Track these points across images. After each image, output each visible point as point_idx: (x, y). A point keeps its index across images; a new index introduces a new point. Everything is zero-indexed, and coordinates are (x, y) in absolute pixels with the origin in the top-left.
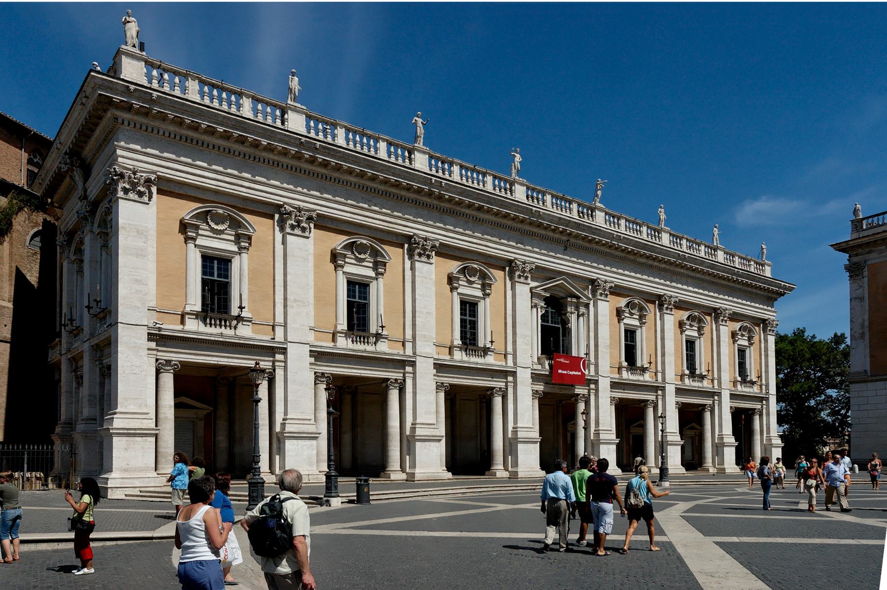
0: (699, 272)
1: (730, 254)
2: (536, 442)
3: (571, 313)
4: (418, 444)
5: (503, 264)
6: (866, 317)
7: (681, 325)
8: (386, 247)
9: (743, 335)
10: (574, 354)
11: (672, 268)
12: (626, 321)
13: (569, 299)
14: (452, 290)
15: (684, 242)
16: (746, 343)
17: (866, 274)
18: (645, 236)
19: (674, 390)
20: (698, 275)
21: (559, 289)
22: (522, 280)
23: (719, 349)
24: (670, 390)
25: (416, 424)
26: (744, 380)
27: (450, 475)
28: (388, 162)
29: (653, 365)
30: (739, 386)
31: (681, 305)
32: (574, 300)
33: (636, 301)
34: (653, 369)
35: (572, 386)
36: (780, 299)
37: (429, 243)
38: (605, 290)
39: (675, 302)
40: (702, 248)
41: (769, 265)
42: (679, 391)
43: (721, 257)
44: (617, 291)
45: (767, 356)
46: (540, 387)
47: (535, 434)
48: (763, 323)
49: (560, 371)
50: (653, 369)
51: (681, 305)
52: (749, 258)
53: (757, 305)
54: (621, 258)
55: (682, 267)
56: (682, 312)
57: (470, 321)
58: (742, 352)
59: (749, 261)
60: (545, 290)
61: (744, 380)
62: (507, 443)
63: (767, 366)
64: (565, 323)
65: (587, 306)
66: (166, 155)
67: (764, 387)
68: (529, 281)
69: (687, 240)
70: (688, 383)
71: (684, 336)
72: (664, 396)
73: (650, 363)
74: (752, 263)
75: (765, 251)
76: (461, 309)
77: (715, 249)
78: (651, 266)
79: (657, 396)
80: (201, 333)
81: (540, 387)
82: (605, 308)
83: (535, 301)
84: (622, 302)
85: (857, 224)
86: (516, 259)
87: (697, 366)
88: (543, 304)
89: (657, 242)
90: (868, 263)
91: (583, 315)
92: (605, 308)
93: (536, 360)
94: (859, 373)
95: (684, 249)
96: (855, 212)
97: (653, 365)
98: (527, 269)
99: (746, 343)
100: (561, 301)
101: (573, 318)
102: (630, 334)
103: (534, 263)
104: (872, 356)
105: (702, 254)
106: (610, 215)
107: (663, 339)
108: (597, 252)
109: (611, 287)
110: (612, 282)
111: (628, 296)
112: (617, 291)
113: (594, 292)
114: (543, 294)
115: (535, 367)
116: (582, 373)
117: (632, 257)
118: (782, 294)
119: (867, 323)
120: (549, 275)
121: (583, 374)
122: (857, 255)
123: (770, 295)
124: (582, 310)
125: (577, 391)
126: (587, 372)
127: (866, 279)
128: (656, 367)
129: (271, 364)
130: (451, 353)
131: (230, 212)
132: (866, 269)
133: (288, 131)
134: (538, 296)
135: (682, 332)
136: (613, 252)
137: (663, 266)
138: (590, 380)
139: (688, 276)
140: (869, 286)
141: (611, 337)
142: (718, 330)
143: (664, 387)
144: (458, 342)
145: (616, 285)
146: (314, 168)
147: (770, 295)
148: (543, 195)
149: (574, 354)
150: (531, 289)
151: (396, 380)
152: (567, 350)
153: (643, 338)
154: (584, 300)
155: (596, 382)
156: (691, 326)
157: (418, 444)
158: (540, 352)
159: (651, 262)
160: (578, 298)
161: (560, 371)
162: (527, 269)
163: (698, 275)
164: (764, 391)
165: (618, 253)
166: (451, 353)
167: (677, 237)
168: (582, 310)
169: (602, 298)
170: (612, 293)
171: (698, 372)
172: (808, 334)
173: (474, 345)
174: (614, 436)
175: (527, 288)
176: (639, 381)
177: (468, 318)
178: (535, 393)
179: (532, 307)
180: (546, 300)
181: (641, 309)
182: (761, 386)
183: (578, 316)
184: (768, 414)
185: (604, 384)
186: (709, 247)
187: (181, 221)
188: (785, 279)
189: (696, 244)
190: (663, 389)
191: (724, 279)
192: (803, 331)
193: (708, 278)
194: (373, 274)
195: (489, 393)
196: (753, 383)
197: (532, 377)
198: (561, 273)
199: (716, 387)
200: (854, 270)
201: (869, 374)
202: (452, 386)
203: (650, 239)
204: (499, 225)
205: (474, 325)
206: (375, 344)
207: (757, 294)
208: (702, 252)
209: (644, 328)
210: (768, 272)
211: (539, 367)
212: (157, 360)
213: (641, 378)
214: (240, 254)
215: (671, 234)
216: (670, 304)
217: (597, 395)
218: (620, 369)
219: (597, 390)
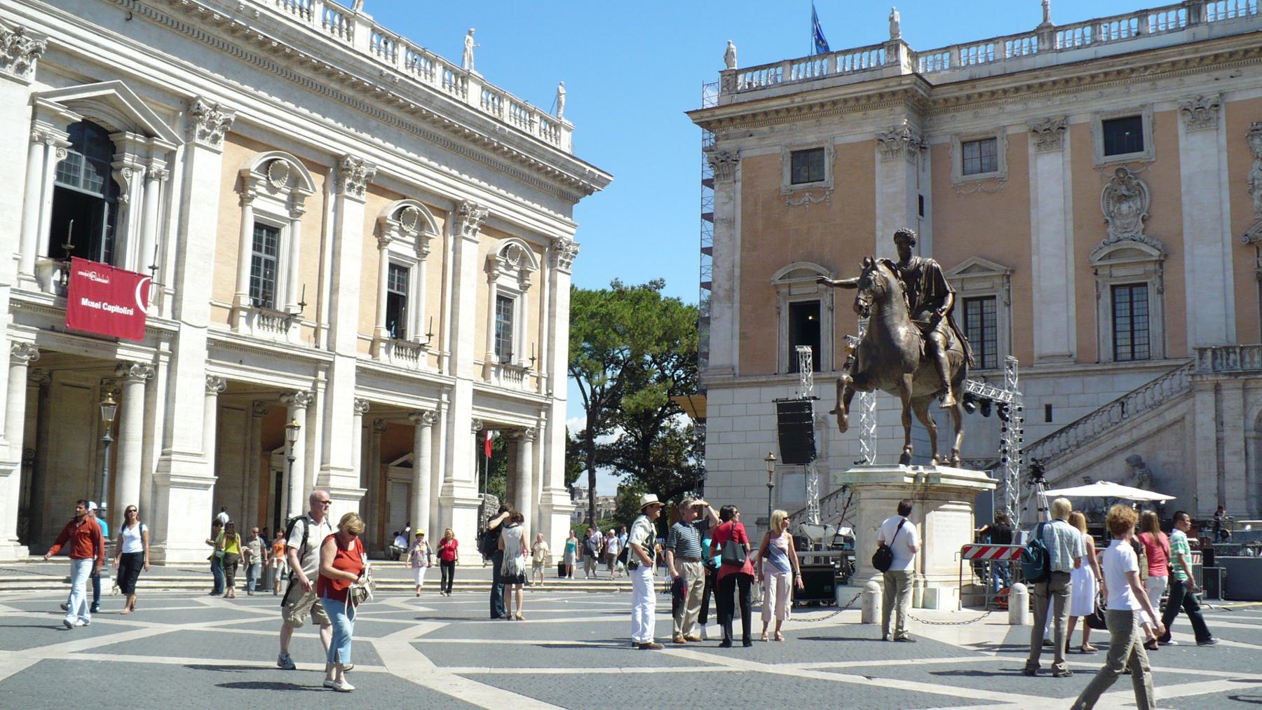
0: (424, 118)
1: (495, 93)
2: (206, 487)
3: (132, 169)
4: (173, 492)
5: (324, 161)
6: (737, 257)
7: (380, 228)
8: (311, 174)
9: (508, 267)
10: (130, 265)
11: (369, 101)
12: (258, 203)
13: (129, 136)
14: (380, 247)
15: (401, 51)
16: (514, 285)
17: (739, 175)
18: (316, 23)
19: (354, 371)
20: (425, 126)
21: (107, 108)
22: (206, 142)
23: (458, 288)
24: (345, 372)
25: (169, 454)
26: (505, 364)
27: (24, 551)
28: (330, 39)
29: (435, 339)
30: (242, 322)
31: (380, 185)
32: (140, 139)
33: (284, 162)
34: (309, 313)
35: (116, 340)
36: (585, 201)
37: (478, 212)
38: (212, 126)
39: (369, 175)
40: (439, 70)
41: (568, 129)
42: (365, 376)
43: (474, 95)
44: (242, 134)
45: (552, 315)
46: (29, 337)
47: (207, 469)
48: (551, 248)
49: (85, 302)
50: (309, 313)
51: (380, 185)
52: (531, 106)
53: (537, 206)
54: (258, 62)
55: (390, 102)
56: (384, 201)
57: (266, 261)
58: (505, 302)
59: (531, 113)
60: (70, 105)
61: (505, 364)
62: (149, 481)
63: (551, 336)
64: (115, 190)
65: (170, 156)
66: (231, 81)
67: (544, 381)
68: (30, 76)
69: (408, 48)
70: (391, 361)
71: (385, 252)
72: (329, 383)
73: (430, 335)
74: (537, 119)
75: (563, 98)
76: (255, 237)
77: (465, 77)
78: (323, 90)
79: (315, 383)
80: (256, 340)
81: (29, 337)
82: (212, 167)
83: (43, 127)
84: (254, 160)
85: (729, 77)
86: (199, 97)
87: (515, 350)
88: (63, 137)
89: (459, 98)
90: (744, 154)
91: (159, 176)
92: (212, 167)
93: (29, 270)
94: (721, 367)
95: (400, 65)
96: (728, 56)
97: (435, 339)
98: (26, 48)
99: (514, 285)
100: (113, 137)
101: (135, 181)
102: (399, 271)
103: (44, 36)
104: (743, 336)
105: (437, 84)
106: (381, 34)
107: (336, 254)
108: (199, 37)
109: (227, 122)
110: (231, 111)
111: (269, 148)
112: (242, 134)
113: (188, 132)
114: (64, 112)
115: (25, 286)
116: (137, 310)
117: (282, 63)
118: (588, 191)
119: (737, 271)
120: (85, 71)
121: (139, 316)
122: (727, 137)
123: (564, 188)
124: (158, 165)
125: (123, 353)
126: (152, 311)
127: (739, 185)
128: (441, 347)
129: (310, 384)
130: (232, 321)
131: (291, 165)
132: (739, 166)
133: (467, 106)
134: (54, 118)
135: (382, 244)
136: (237, 42)
137: (349, 92)
138: (160, 330)
139: (401, 124)
140: (744, 200)
141: (220, 237)
142: (457, 250)
143: (331, 363)
144: (246, 301)
145: (238, 119)
146: (202, 26)
147: (564, 188)
148: (500, 100)
149: (130, 265)
150: (33, 99)
151: (142, 365)
152: (114, 255)
153: (297, 246)
154: (163, 142)
155: (174, 337)
156: (403, 232)
157: (173, 492)
158: (44, 251)
159: (322, 80)
160: (149, 135)
161: (85, 302)
162: (26, 48)
163: (425, 126)
164: (544, 392)
165: (250, 49)
166: (232, 321)
167: (388, 39)
168: (158, 165)
169: (563, 268)
170: (232, 137)
171: (514, 361)
172: (664, 293)
173: (269, 306)
174: (356, 483)
175: (23, 94)
176: (274, 343)
177: (263, 255)
178: (18, 351)
179: (32, 142)
180: (73, 128)
181: (296, 181)
182: (538, 380)
183: (147, 179)
184: (548, 441)
185: (192, 346)
186: (451, 70)
187: (240, 172)
188: (596, 158)
189: (427, 58)
190: (329, 367)
191: (475, 141)
192: (659, 284)
193: (442, 133)
194: (286, 213)
195: (284, 400)
196: (522, 371)
197: (209, 348)
198: (113, 72)
199: (446, 373)
200: (721, 165)
201: (737, 371)
202: (231, 383)
203: (327, 32)
204: (323, 90)
205: (272, 266)
206: (286, 331)
207: (540, 183)
208: (437, 80)
209: (298, 224)
210: (565, 142)
211: (35, 288)
212: (13, 342)
213: (280, 337)
214: (292, 221)
215: (374, 30)
216: (358, 179)
217: (328, 391)
218: (485, 368)
219: (173, 356)
